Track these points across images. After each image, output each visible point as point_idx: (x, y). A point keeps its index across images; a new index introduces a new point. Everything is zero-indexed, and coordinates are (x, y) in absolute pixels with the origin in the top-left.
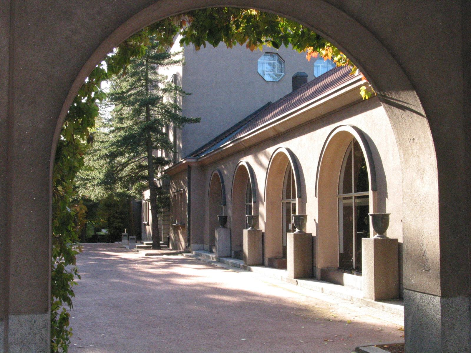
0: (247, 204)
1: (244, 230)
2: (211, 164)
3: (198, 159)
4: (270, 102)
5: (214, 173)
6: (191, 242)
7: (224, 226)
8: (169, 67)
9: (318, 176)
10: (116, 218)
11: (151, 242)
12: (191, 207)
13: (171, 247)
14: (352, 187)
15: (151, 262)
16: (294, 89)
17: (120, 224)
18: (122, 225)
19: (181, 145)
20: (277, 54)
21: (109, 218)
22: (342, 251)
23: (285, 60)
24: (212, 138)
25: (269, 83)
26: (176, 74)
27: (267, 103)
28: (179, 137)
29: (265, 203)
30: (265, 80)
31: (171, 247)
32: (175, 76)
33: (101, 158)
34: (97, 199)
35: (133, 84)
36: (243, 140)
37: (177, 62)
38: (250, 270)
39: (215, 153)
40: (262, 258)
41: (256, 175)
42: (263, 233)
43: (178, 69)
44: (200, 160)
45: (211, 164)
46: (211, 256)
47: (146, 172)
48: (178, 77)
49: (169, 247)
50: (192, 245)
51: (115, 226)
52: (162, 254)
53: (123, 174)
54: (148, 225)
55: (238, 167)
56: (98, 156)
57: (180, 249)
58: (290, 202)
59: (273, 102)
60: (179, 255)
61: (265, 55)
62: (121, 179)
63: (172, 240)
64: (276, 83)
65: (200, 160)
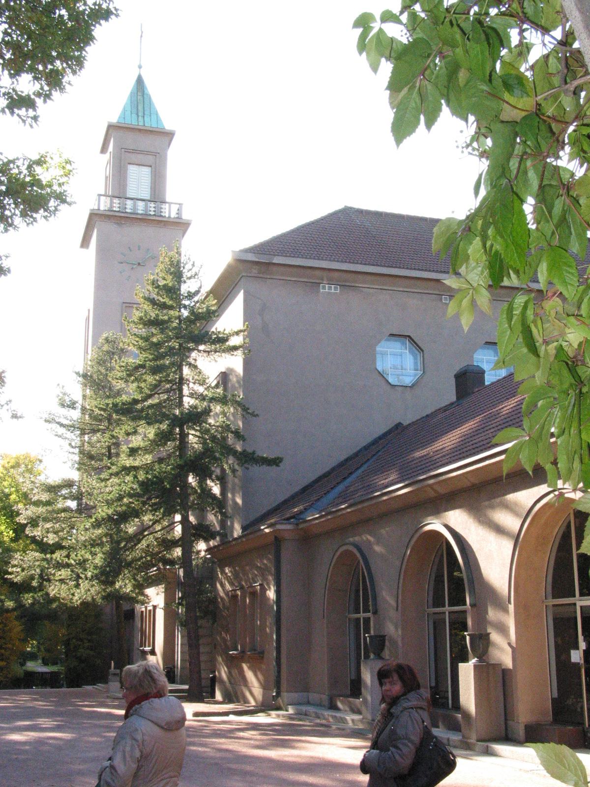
0: (429, 609)
1: (460, 664)
2: (329, 534)
3: (297, 524)
4: (400, 423)
5: (344, 548)
6: (284, 685)
7: (379, 655)
8: (218, 359)
9: (517, 553)
10: (81, 640)
11: (186, 687)
12: (282, 617)
13: (219, 696)
14: (448, 578)
15: (232, 731)
16: (458, 398)
17: (88, 652)
18: (92, 653)
19: (239, 501)
20: (409, 336)
21: (69, 640)
22: (556, 695)
23: (424, 349)
24: (297, 489)
25: (396, 388)
26: (225, 372)
27: (393, 425)
28: (234, 485)
29: (511, 607)
30: (389, 383)
31: (219, 696)
32: (224, 377)
33: (97, 525)
34: (83, 603)
35: (156, 386)
36: (444, 477)
37: (235, 348)
38: (492, 754)
39: (349, 510)
40: (503, 723)
41: (475, 550)
42: (505, 672)
43: (235, 363)
44: (301, 526)
45: (329, 534)
46: (348, 718)
47: (178, 552)
48: (231, 377)
49: (213, 695)
50: (285, 695)
51: (79, 654)
52: (226, 714)
53: (137, 553)
54: (153, 652)
55: (417, 535)
56: (94, 520)
57: (246, 701)
58: (575, 604)
59: (405, 424)
60: (259, 714)
61: (387, 340)
62: (129, 565)
63: (222, 682)
64: (409, 389)
65: (301, 526)
